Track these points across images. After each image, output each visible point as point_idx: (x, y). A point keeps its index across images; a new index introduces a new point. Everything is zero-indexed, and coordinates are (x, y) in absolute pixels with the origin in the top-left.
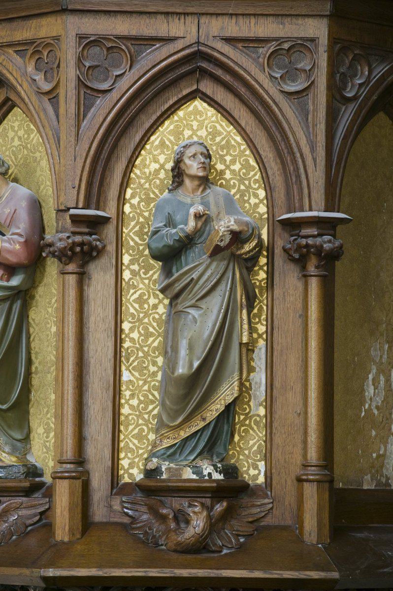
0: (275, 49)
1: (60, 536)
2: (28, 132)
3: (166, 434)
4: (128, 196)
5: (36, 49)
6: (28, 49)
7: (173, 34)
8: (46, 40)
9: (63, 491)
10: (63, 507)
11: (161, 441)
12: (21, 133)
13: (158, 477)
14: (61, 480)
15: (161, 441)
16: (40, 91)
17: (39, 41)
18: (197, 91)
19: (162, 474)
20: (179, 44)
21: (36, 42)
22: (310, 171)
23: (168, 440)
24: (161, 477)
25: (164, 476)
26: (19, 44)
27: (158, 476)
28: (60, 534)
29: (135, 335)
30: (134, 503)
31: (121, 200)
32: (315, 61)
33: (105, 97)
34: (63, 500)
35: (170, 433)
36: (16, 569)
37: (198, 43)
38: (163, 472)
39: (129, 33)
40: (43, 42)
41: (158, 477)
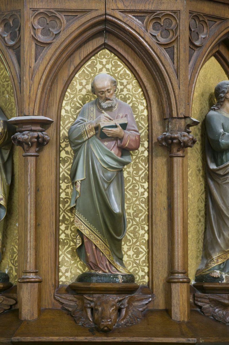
0: (153, 17)
1: (182, 318)
2: (116, 66)
3: (221, 256)
4: (64, 104)
5: (156, 17)
6: (146, 16)
7: (88, 7)
8: (165, 11)
9: (183, 290)
10: (184, 300)
11: (217, 260)
12: (109, 66)
13: (220, 282)
14: (182, 284)
15: (217, 260)
16: (159, 43)
17: (158, 12)
18: (105, 44)
19: (223, 280)
20: (94, 14)
21: (157, 12)
22: (177, 91)
23: (221, 260)
24: (222, 281)
25: (224, 281)
26: (141, 12)
27: (220, 281)
28: (182, 317)
29: (141, 190)
30: (201, 298)
31: (60, 108)
32: (178, 24)
33: (48, 47)
34: (184, 295)
35: (222, 256)
36: (173, 338)
37: (106, 14)
38: (224, 279)
39: (166, 8)
40: (162, 13)
41: (220, 282)
